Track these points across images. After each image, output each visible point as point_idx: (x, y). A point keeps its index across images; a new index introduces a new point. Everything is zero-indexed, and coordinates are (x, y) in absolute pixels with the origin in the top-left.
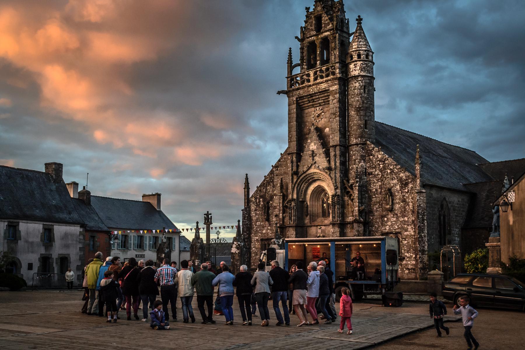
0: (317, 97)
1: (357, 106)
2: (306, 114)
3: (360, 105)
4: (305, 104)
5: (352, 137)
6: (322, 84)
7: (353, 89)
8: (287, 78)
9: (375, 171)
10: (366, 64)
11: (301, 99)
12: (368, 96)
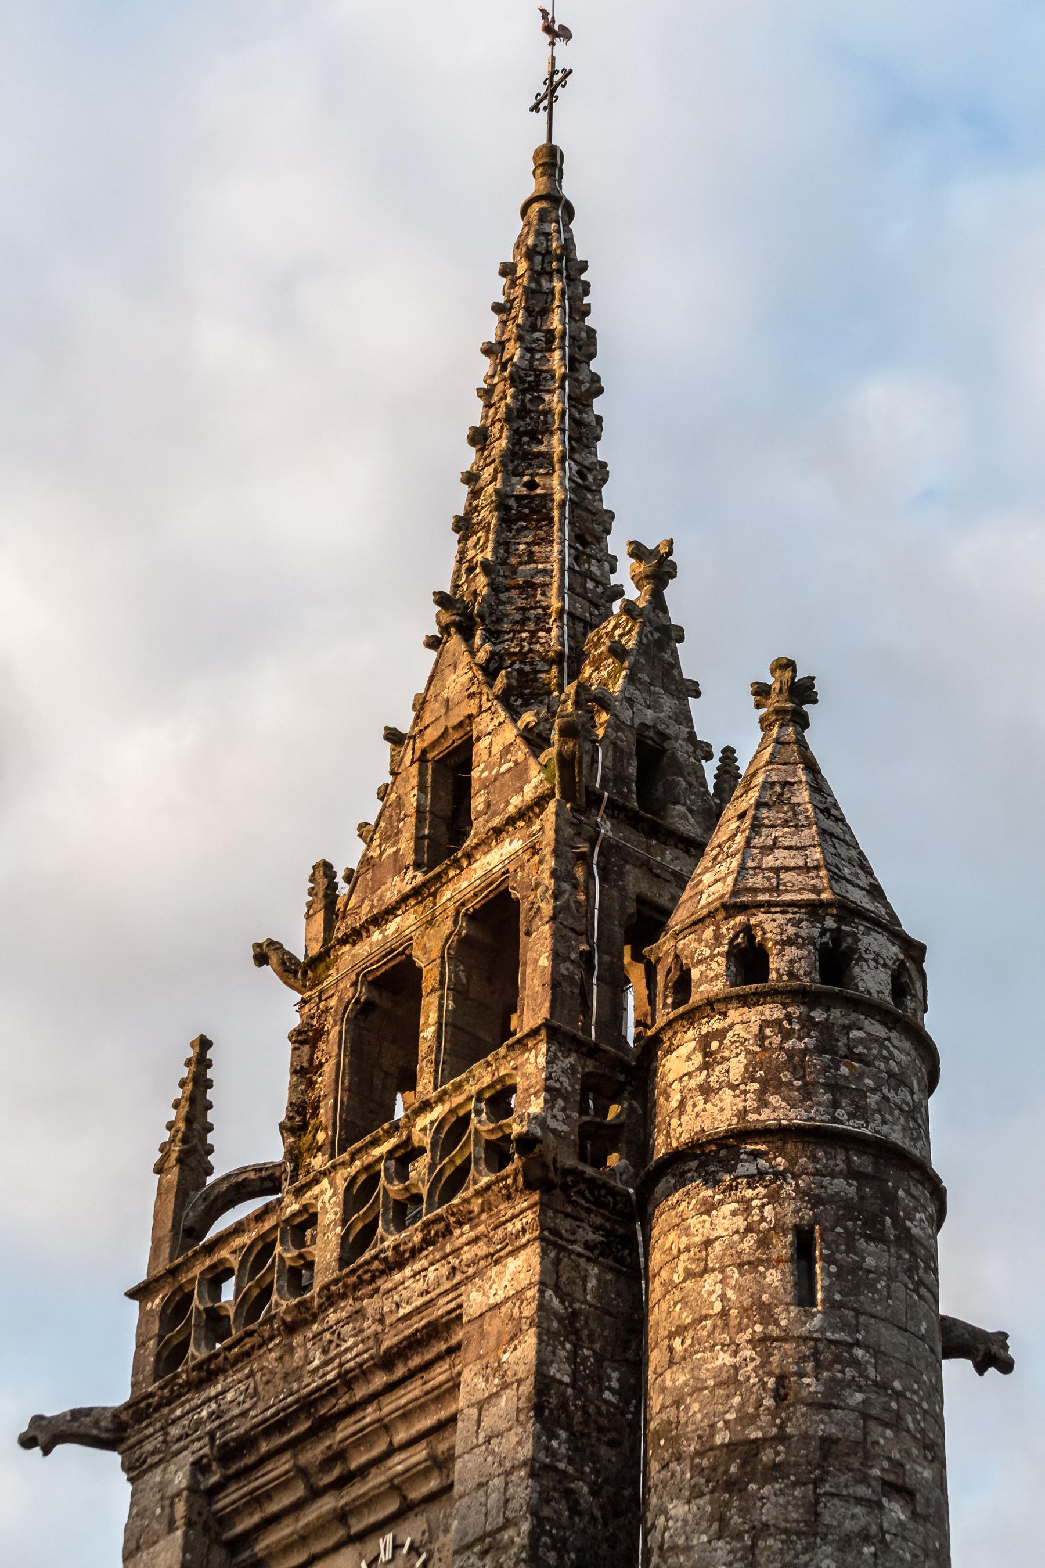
0: (370, 1414)
1: (721, 1438)
3: (746, 1419)
6: (398, 1277)
7: (689, 1274)
8: (139, 1293)
10: (825, 1027)
12: (845, 1326)
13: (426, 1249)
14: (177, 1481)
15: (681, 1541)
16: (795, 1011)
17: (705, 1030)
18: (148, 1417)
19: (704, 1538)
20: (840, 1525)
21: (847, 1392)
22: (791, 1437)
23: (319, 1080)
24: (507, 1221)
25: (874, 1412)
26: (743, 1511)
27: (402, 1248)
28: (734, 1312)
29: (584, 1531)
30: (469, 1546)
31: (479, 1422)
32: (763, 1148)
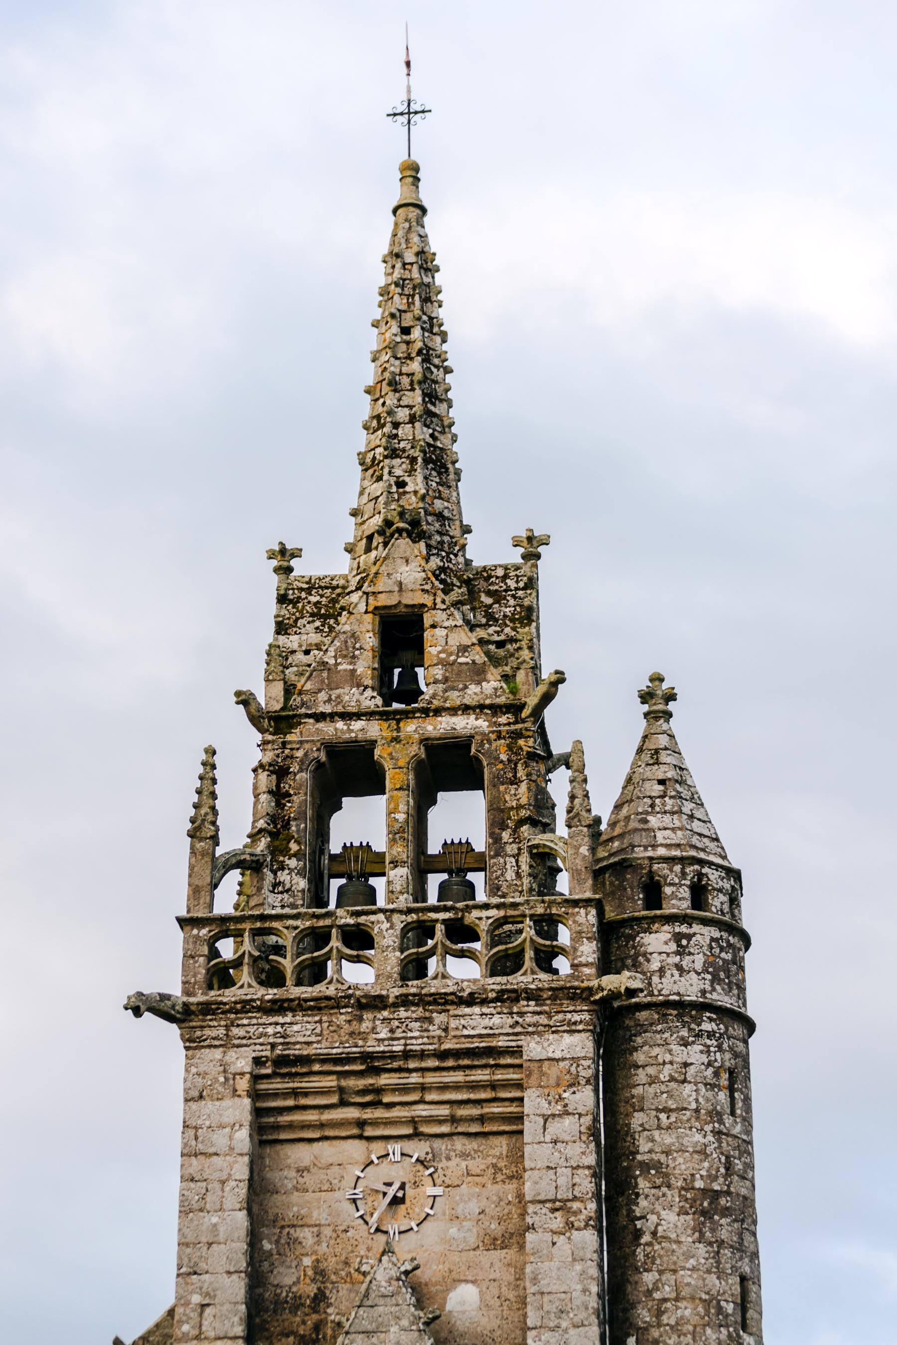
0: (415, 1078)
1: (699, 1184)
2: (301, 1171)
4: (305, 1108)
6: (467, 1010)
7: (672, 1079)
11: (283, 1076)
13: (495, 1003)
15: (673, 1236)
16: (725, 935)
17: (677, 930)
18: (213, 1014)
19: (690, 1239)
22: (732, 1193)
23: (288, 805)
24: (568, 1012)
26: (713, 1230)
27: (476, 996)
28: (703, 1112)
32: (714, 1016)
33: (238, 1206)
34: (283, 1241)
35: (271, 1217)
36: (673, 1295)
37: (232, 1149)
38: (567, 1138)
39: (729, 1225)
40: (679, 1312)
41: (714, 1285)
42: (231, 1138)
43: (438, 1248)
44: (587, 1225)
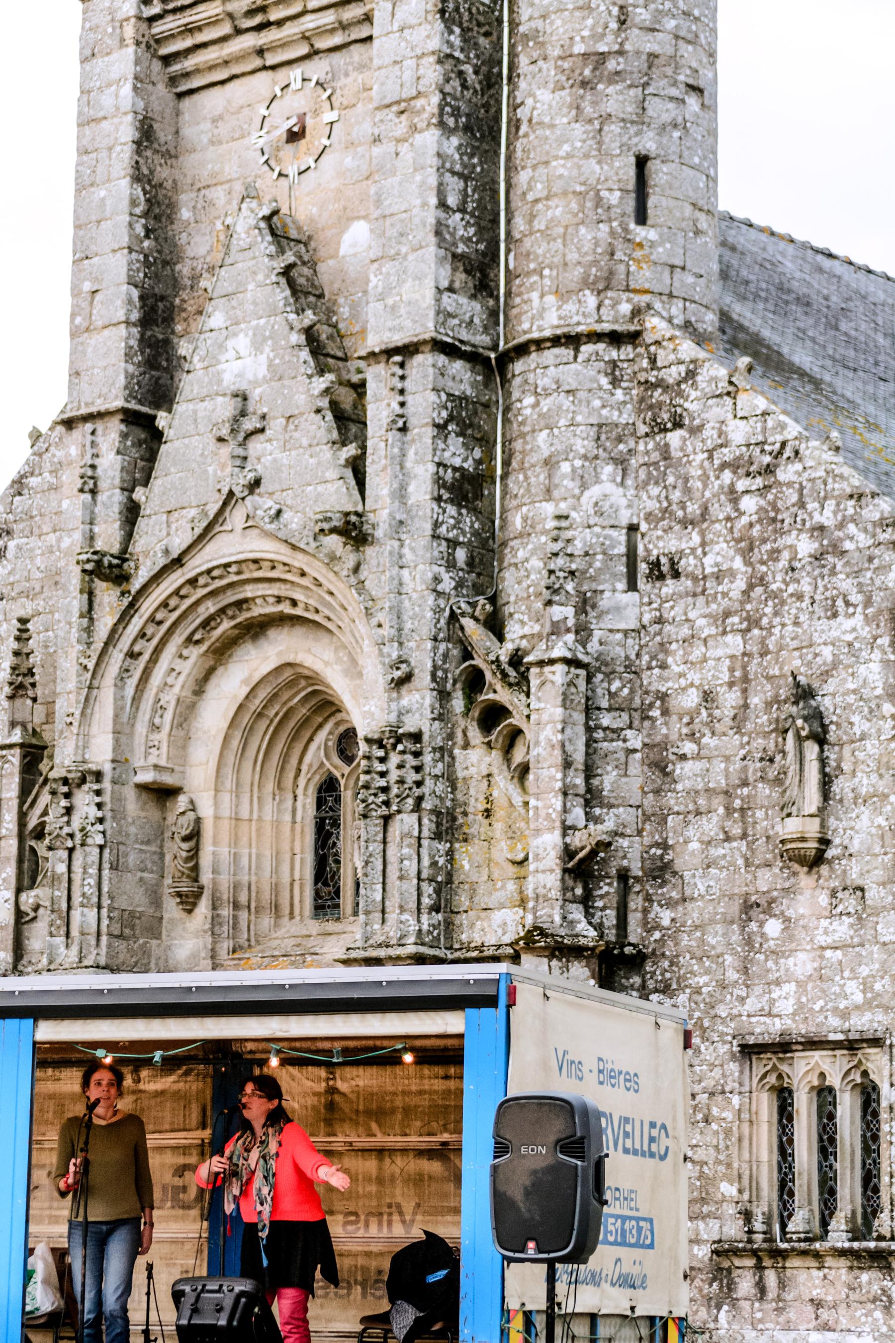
1: (579, 48)
4: (204, 45)
5: (532, 289)
9: (703, 544)
14: (125, 9)
15: (547, 120)
19: (565, 120)
20: (659, 116)
21: (665, 20)
25: (682, 33)
26: (594, 103)
29: (470, 101)
30: (389, 106)
31: (393, 15)
33: (123, 173)
34: (199, 206)
35: (189, 181)
36: (545, 193)
37: (118, 109)
38: (414, 21)
39: (621, 92)
40: (550, 213)
41: (593, 172)
42: (117, 96)
43: (334, 185)
44: (429, 125)
